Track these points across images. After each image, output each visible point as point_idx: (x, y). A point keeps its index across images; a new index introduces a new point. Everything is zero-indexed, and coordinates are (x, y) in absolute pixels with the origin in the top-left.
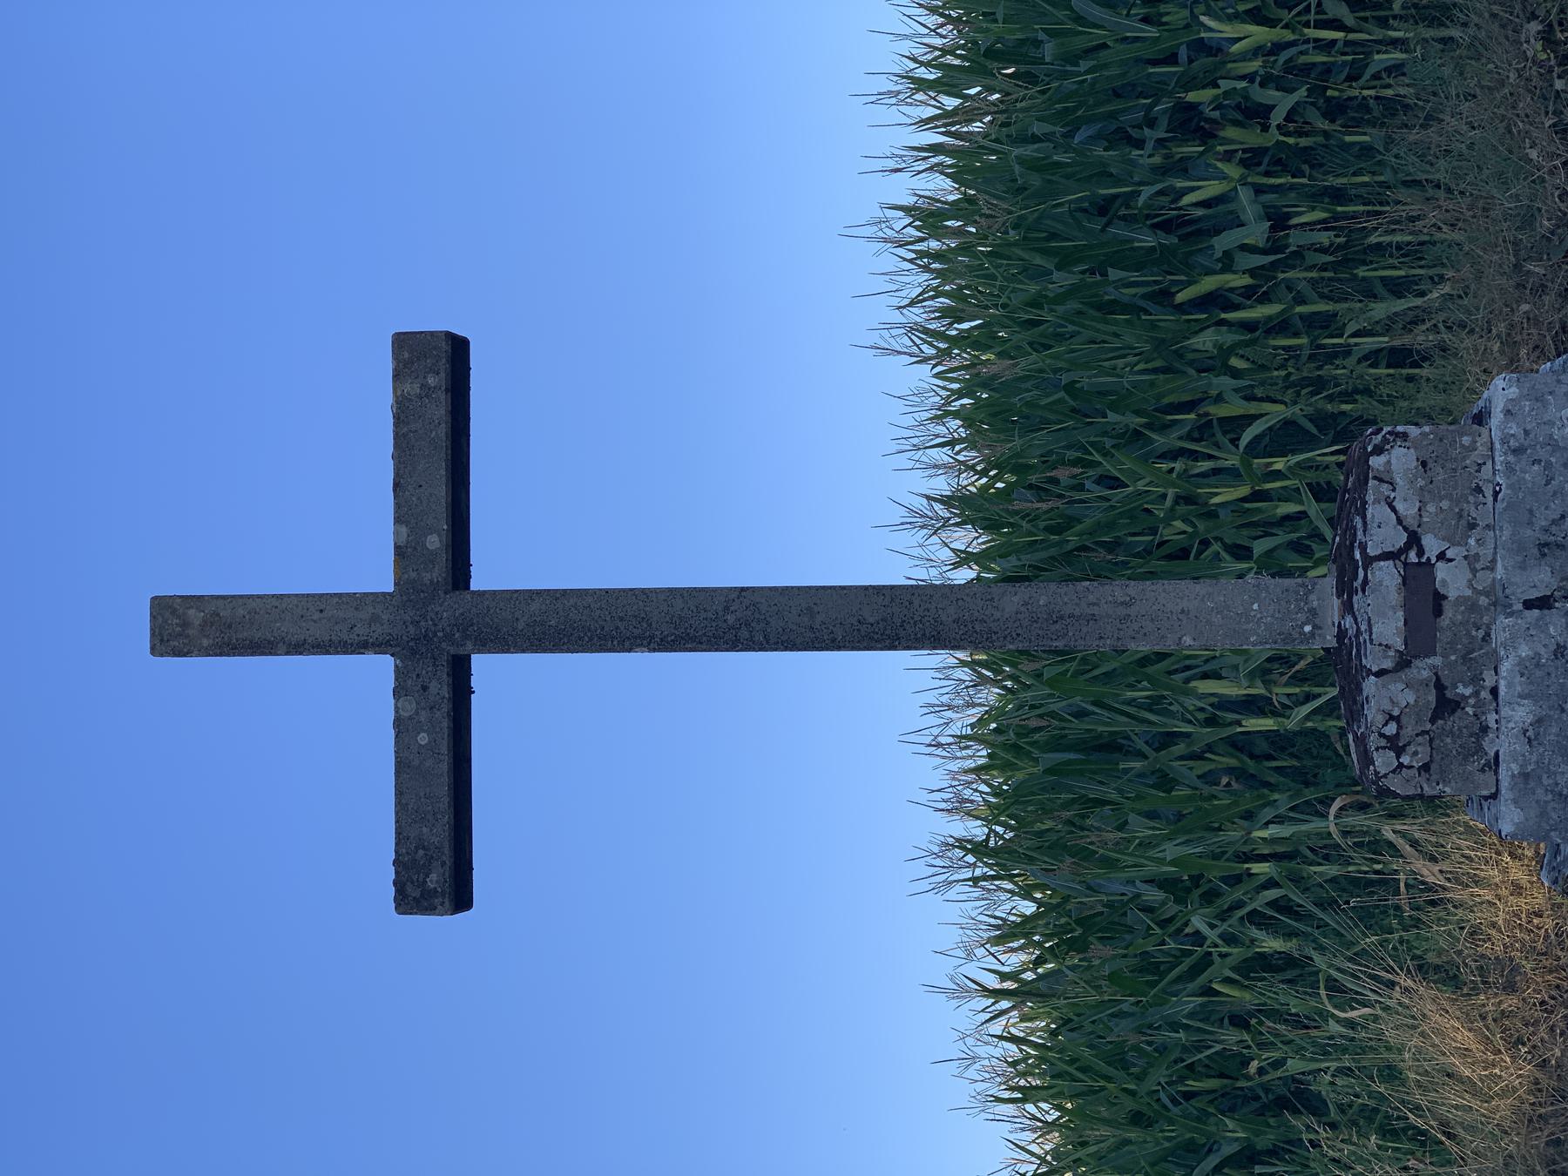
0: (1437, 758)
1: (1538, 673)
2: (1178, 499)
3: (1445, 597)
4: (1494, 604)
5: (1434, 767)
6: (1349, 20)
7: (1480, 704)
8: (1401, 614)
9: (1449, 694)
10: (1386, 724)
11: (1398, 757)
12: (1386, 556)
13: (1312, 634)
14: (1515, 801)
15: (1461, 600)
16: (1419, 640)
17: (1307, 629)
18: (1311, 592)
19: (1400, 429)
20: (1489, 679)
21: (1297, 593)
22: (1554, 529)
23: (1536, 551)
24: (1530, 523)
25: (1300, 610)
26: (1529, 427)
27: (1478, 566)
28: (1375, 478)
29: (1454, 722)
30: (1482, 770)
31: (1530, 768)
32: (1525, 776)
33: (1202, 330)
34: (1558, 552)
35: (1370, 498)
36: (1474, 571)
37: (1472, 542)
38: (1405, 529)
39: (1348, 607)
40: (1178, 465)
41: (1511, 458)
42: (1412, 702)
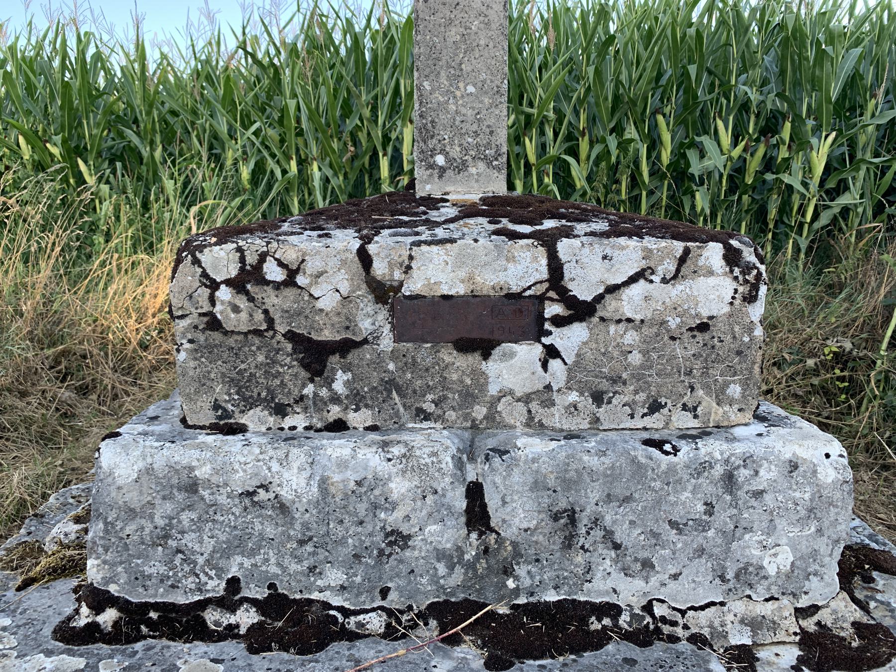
0: (231, 341)
1: (362, 508)
2: (528, 117)
3: (486, 356)
4: (474, 427)
5: (217, 336)
6: (817, 225)
7: (319, 404)
8: (460, 289)
9: (334, 359)
10: (280, 264)
11: (228, 282)
12: (556, 268)
13: (431, 166)
14: (149, 471)
15: (481, 379)
16: (423, 319)
17: (440, 160)
18: (489, 164)
19: (763, 289)
20: (358, 419)
21: (488, 145)
22: (598, 534)
23: (563, 504)
24: (609, 498)
25: (465, 150)
26: (768, 498)
27: (534, 406)
28: (687, 251)
29: (290, 368)
30: (216, 407)
31: (205, 493)
32: (192, 487)
33: (638, 132)
34: (558, 539)
35: (650, 242)
36: (527, 399)
37: (573, 397)
38: (599, 298)
39: (468, 211)
40: (551, 115)
41: (719, 470)
42: (320, 304)
